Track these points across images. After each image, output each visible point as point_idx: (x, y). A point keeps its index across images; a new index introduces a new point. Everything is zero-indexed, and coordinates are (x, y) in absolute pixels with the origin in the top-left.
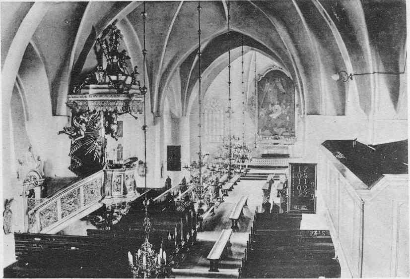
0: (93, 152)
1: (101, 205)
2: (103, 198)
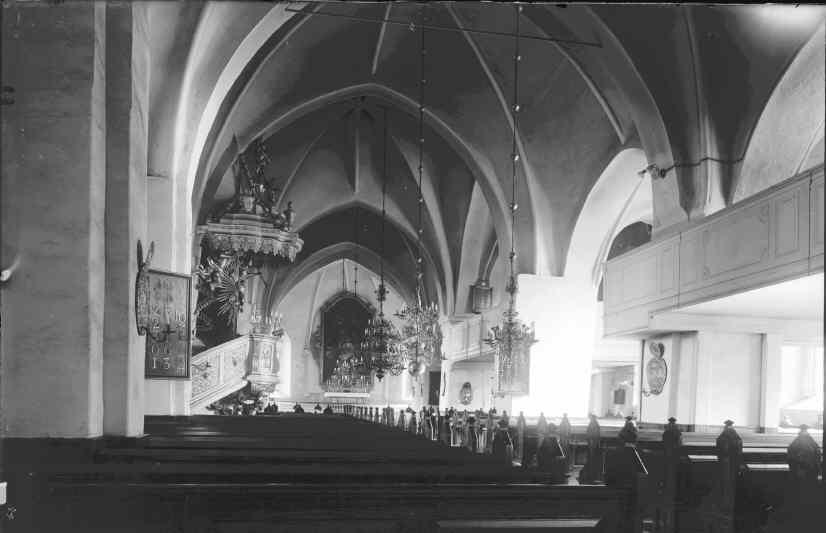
0: (228, 313)
1: (245, 383)
2: (248, 374)
